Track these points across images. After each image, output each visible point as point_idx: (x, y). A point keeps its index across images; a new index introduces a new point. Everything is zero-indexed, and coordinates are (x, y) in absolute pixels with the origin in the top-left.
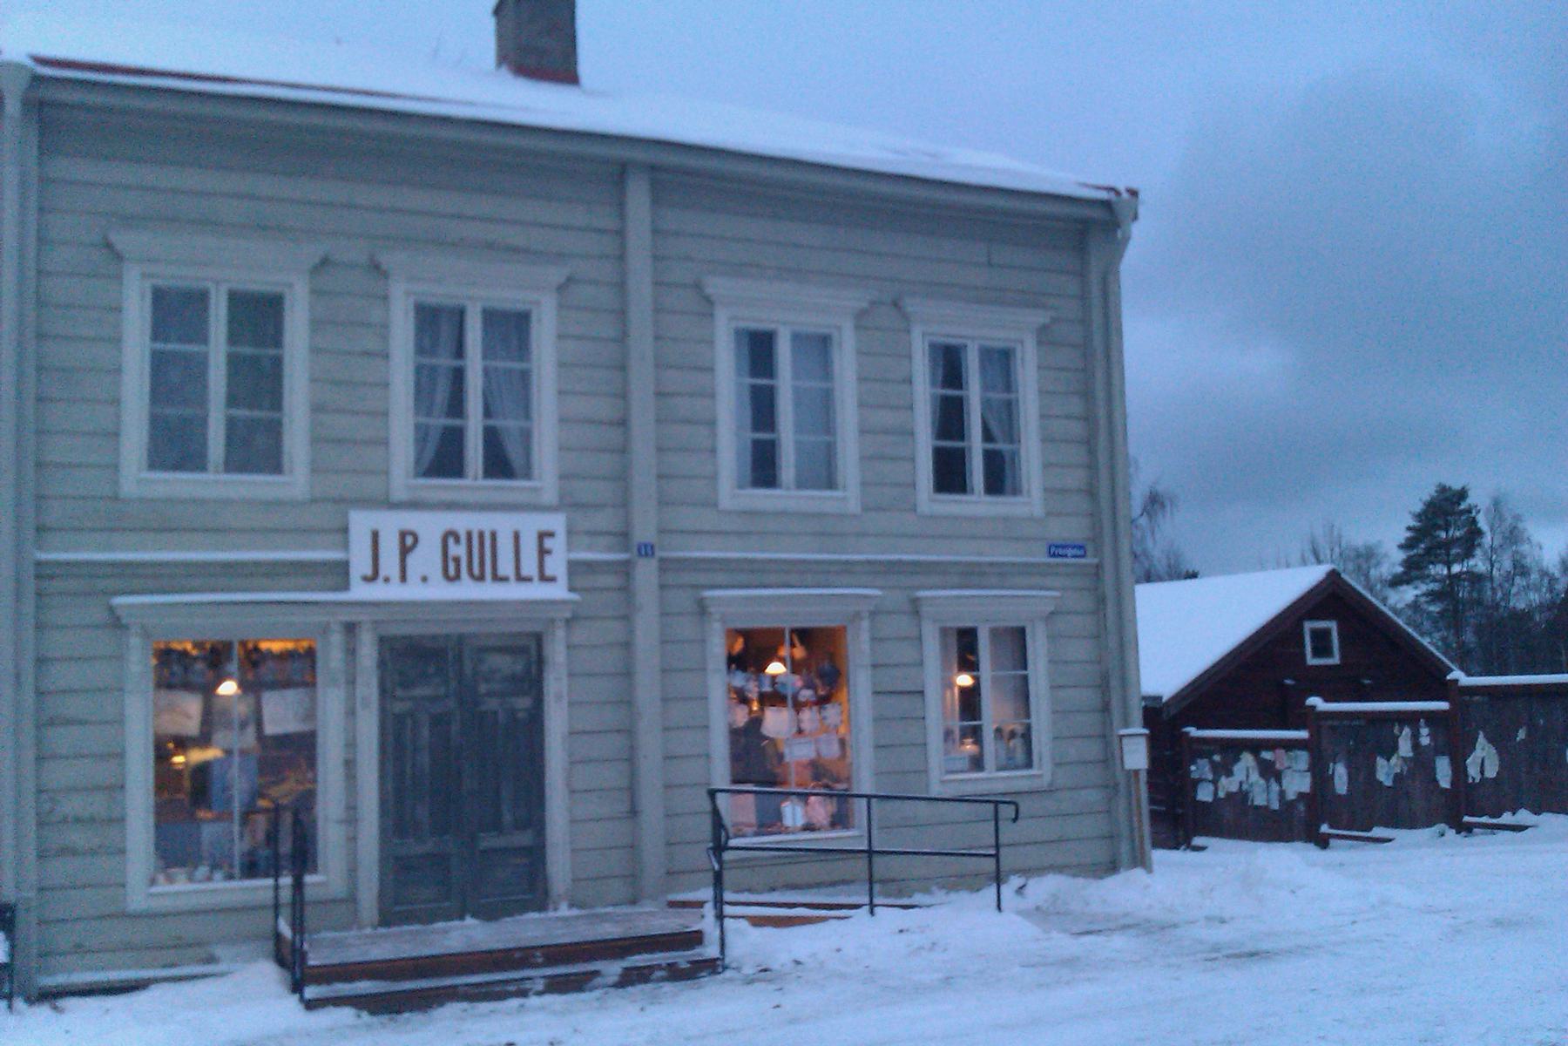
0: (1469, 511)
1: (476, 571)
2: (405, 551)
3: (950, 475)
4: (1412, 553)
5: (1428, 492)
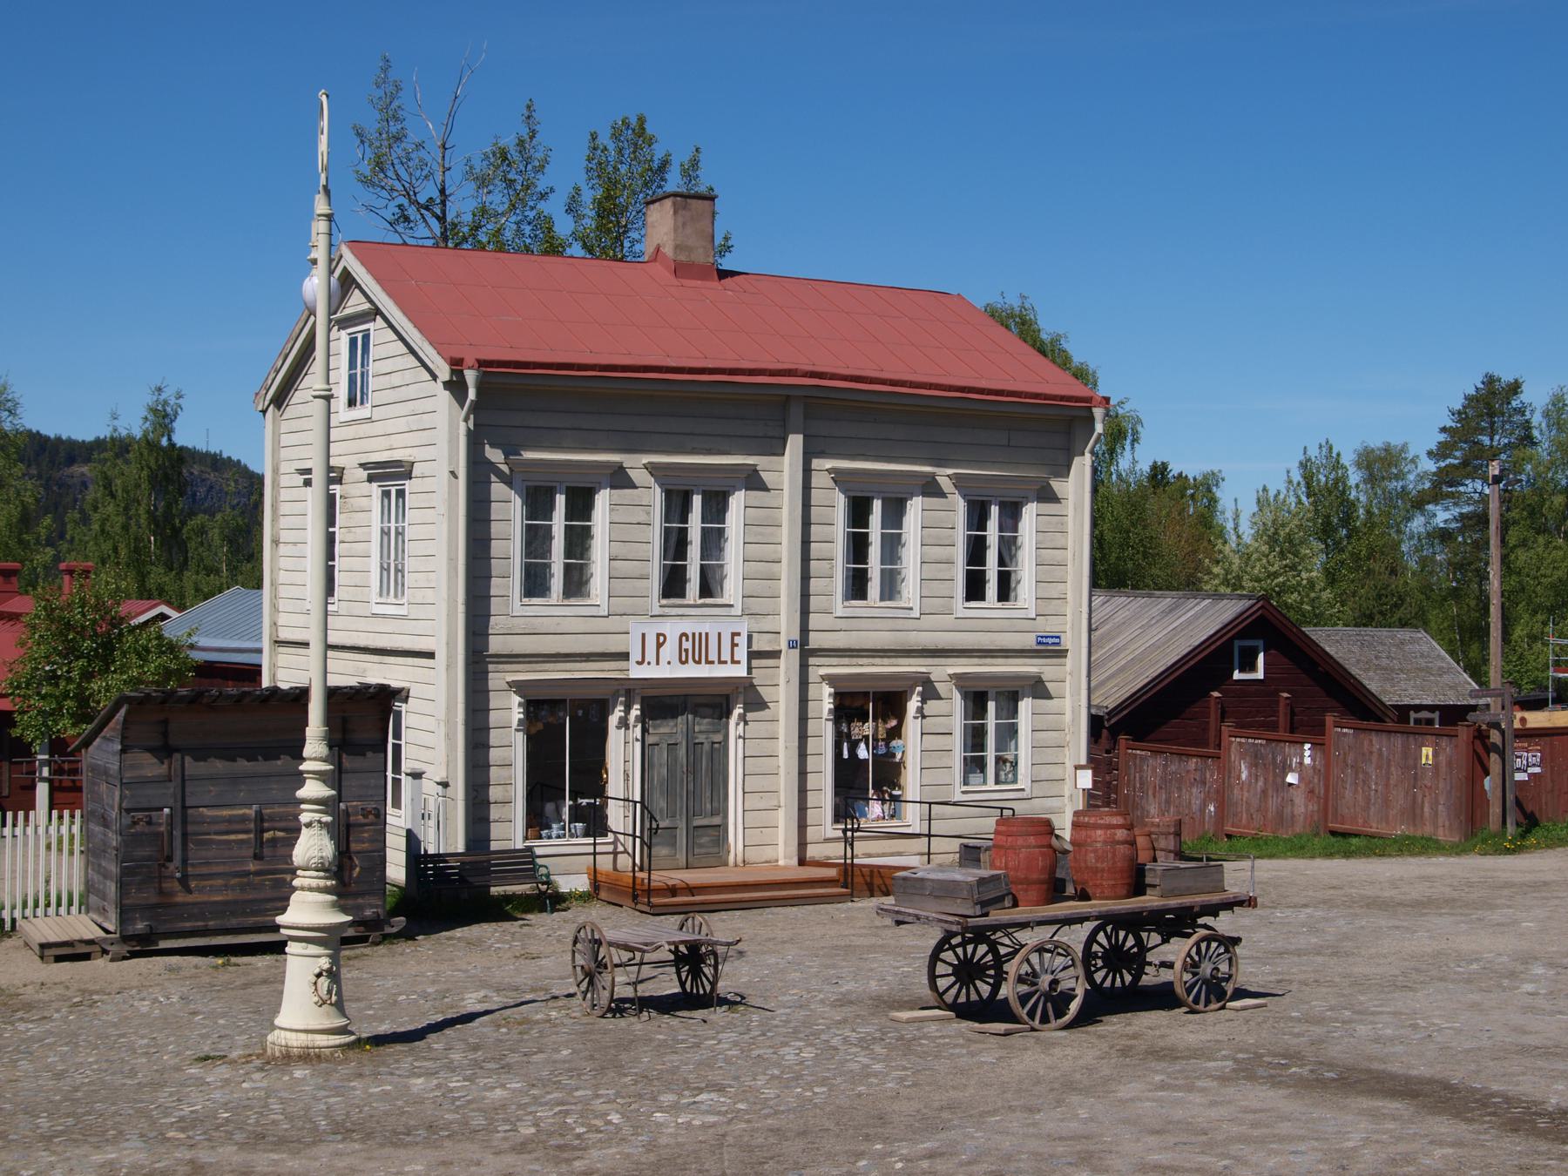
0: (1521, 411)
1: (697, 659)
2: (659, 645)
3: (975, 589)
4: (1442, 464)
5: (1470, 384)
